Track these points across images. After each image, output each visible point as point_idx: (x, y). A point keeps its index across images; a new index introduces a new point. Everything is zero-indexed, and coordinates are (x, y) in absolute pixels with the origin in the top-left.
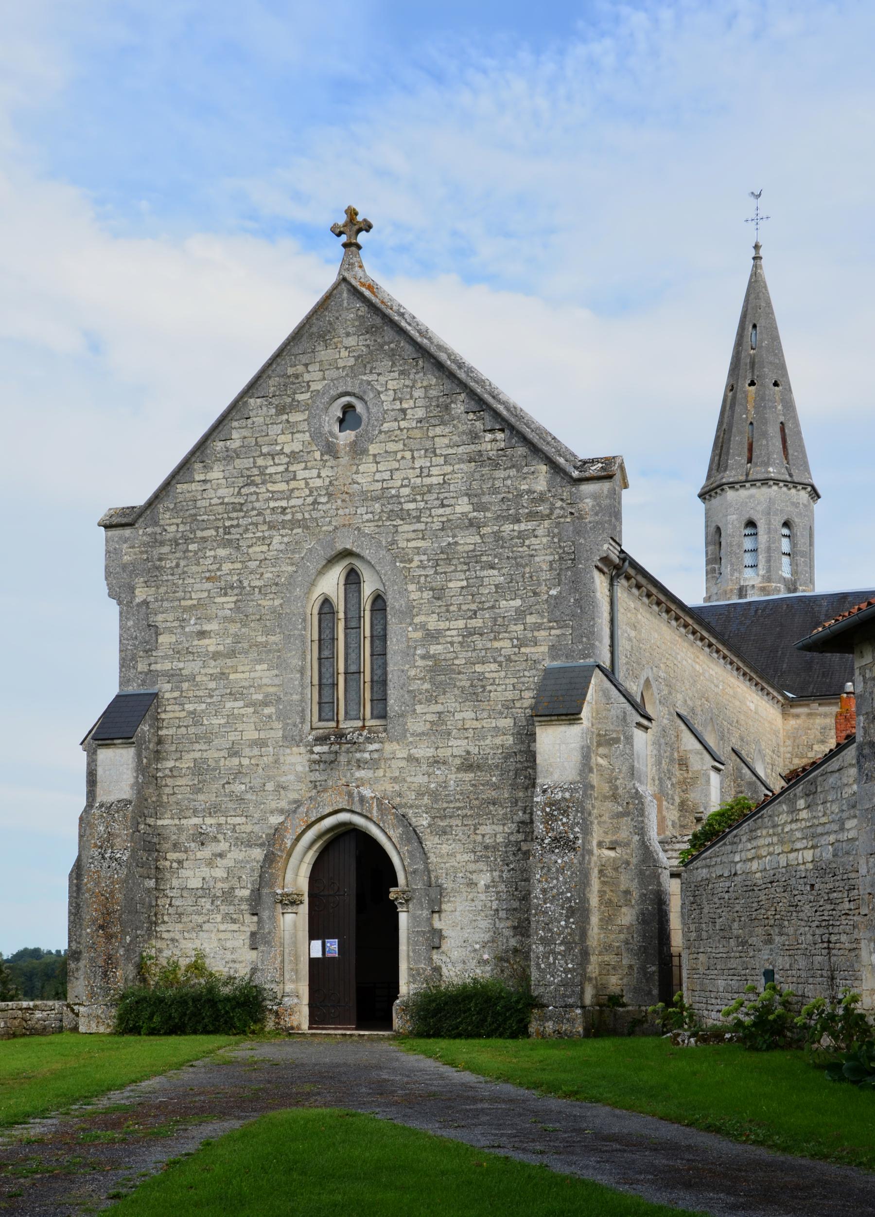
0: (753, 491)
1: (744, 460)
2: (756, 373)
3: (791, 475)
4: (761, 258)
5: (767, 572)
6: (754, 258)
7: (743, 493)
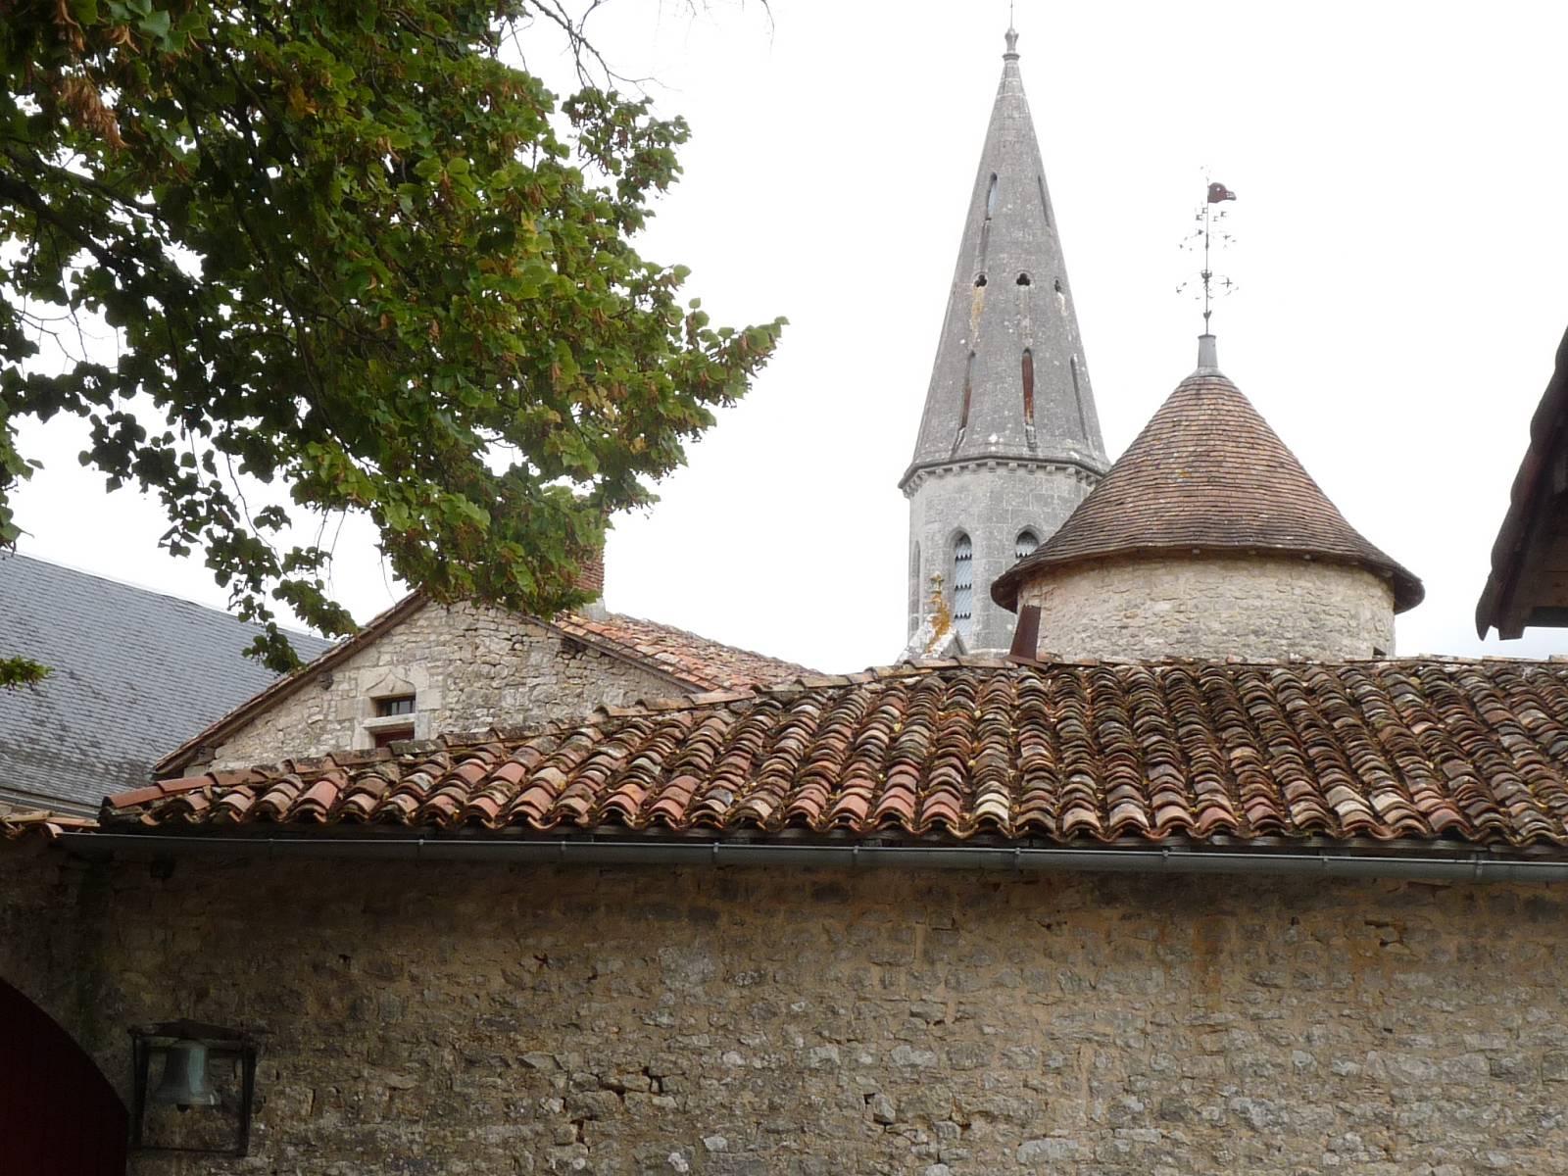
0: (967, 477)
1: (954, 424)
2: (989, 263)
3: (1032, 447)
4: (1016, 57)
5: (984, 628)
6: (1006, 57)
7: (951, 481)
